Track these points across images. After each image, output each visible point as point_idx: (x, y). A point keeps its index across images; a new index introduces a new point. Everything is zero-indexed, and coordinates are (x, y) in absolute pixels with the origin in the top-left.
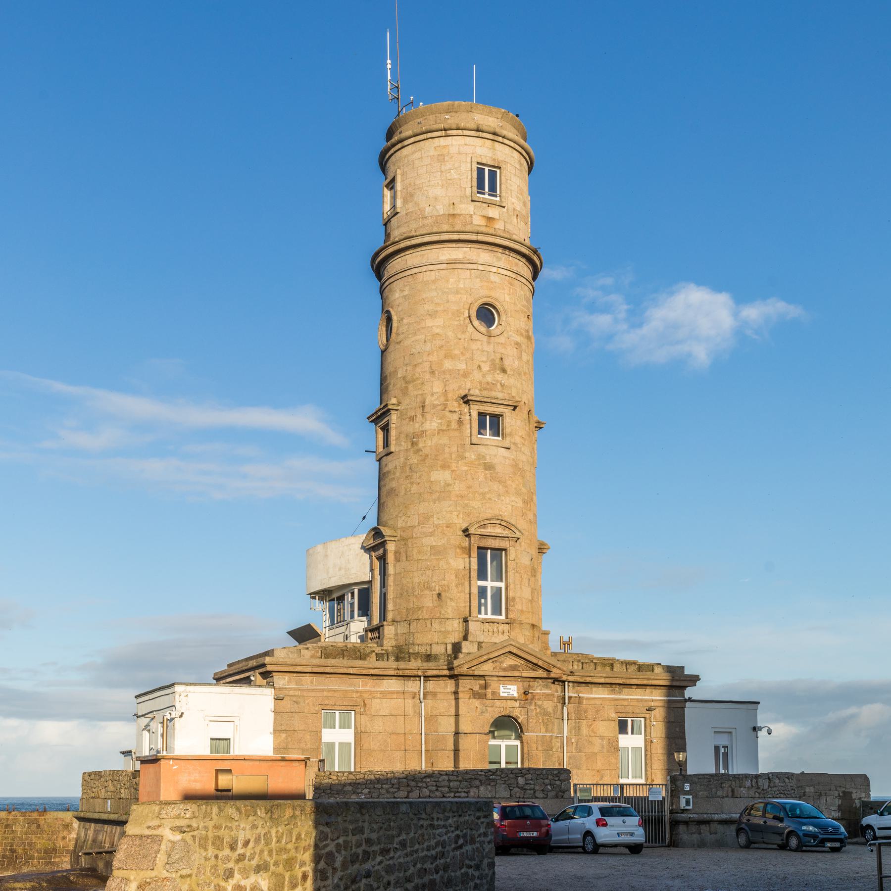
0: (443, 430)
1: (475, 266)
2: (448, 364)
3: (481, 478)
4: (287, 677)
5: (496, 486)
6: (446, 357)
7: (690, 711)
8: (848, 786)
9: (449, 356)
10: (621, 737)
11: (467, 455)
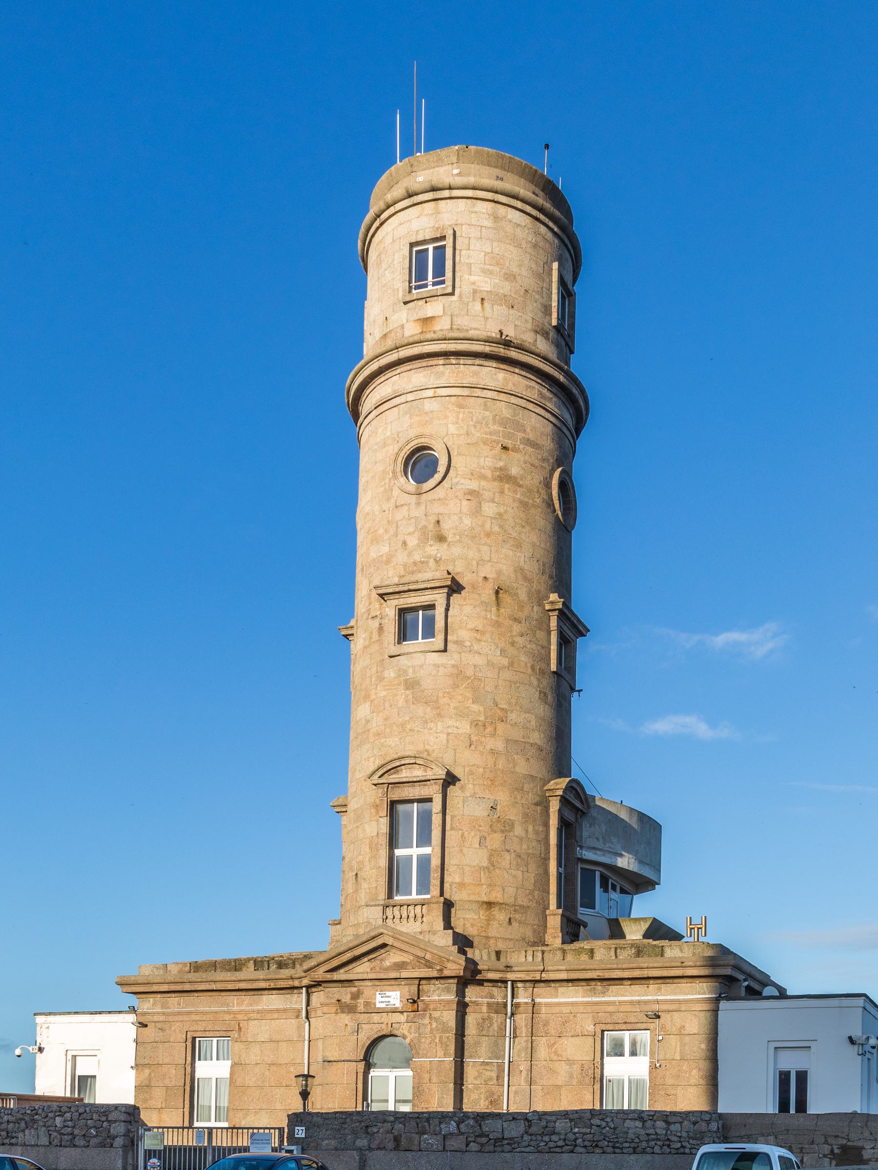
3: (401, 702)
4: (151, 999)
5: (420, 710)
8: (852, 1136)
11: (386, 674)
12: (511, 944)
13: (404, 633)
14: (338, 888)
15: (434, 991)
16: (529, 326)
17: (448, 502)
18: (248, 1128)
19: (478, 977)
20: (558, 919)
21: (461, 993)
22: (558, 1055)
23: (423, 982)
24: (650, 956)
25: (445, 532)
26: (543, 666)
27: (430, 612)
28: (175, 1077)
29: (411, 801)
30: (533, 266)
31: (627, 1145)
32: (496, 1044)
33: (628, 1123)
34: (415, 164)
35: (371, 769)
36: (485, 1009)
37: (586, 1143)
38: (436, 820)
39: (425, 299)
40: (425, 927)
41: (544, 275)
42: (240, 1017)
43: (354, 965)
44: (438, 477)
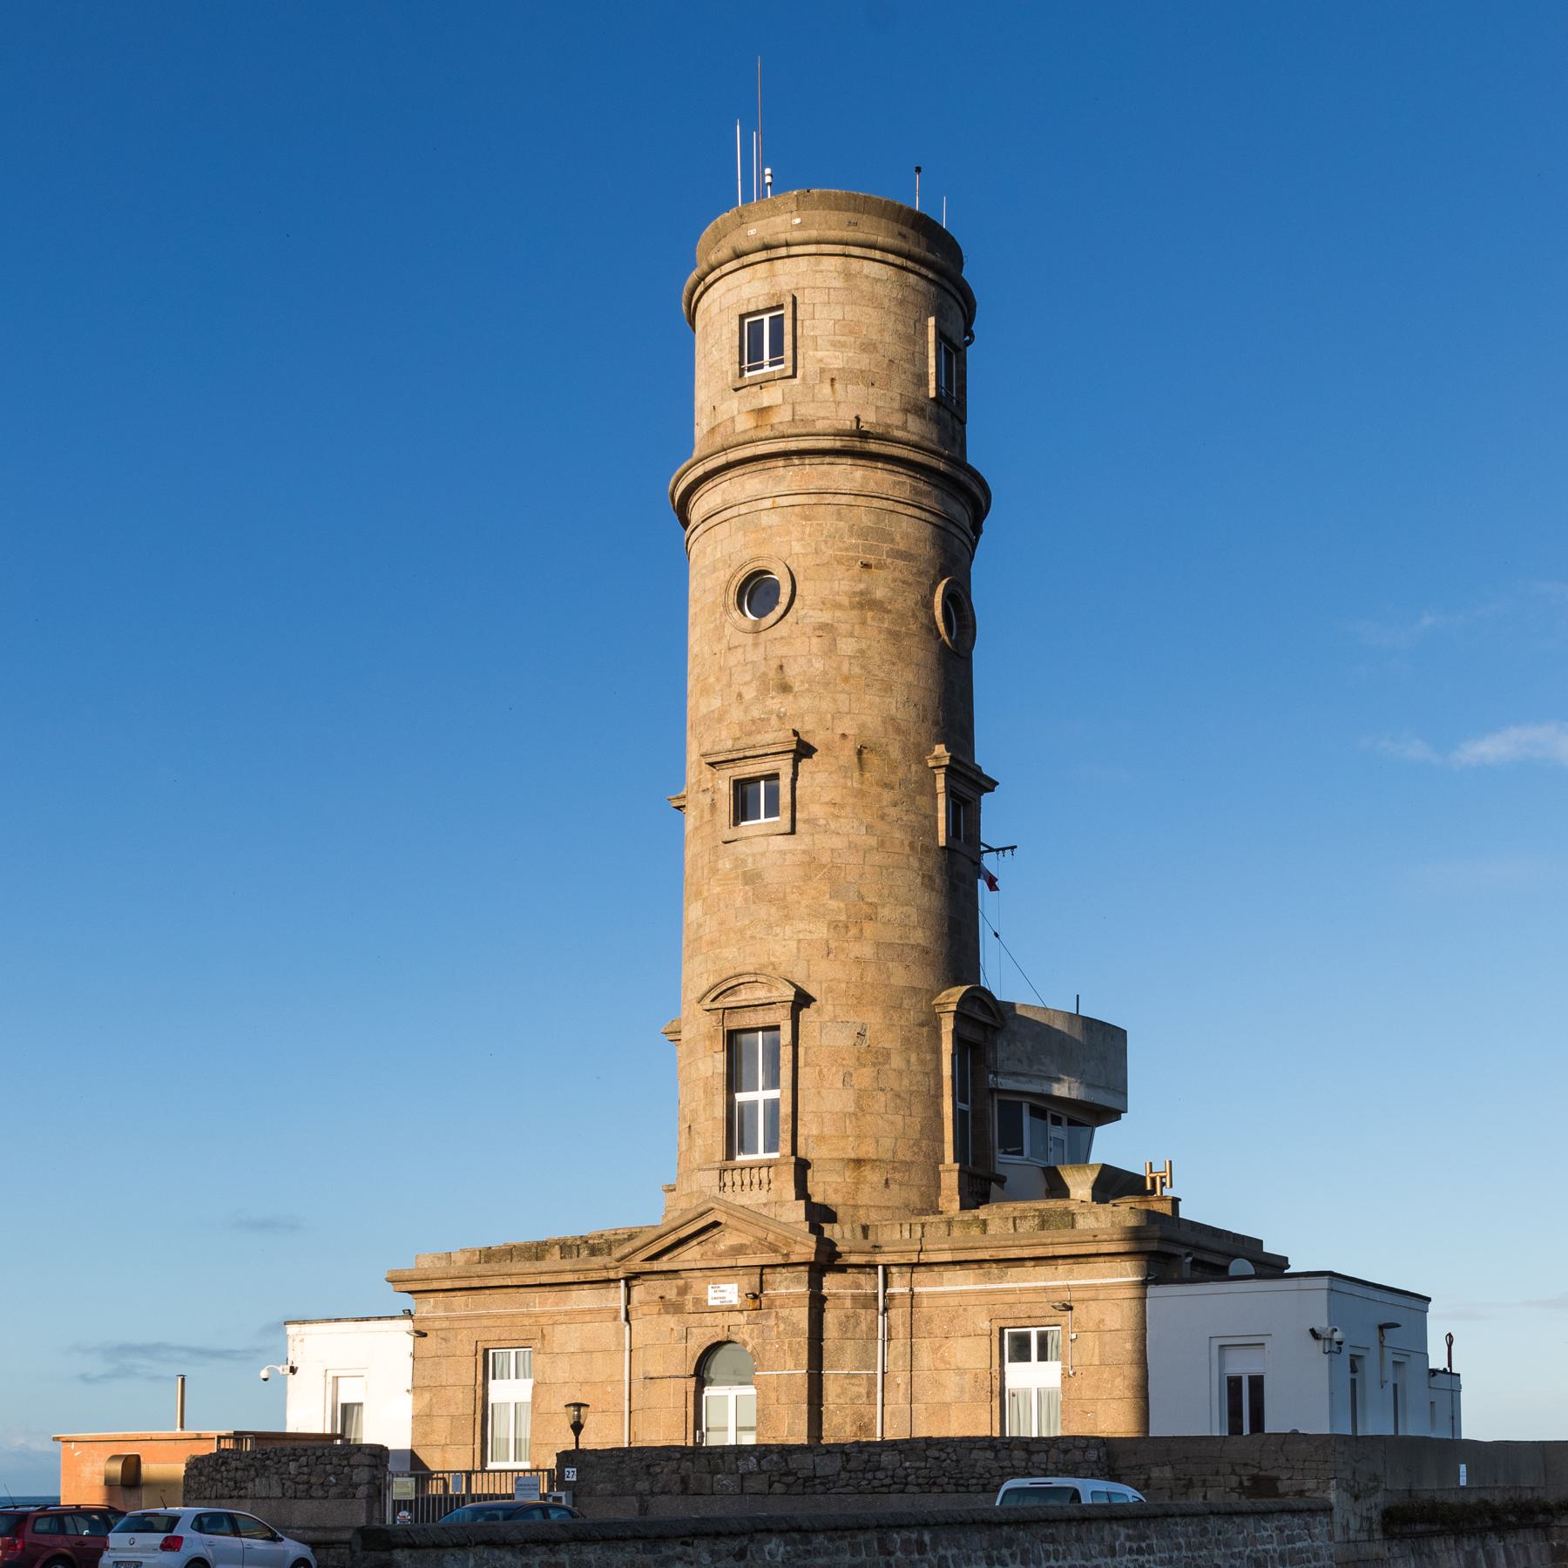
3: (739, 902)
4: (431, 1299)
5: (762, 911)
10: (1012, 1369)
11: (720, 866)
12: (888, 1214)
13: (743, 808)
14: (643, 1153)
16: (896, 405)
17: (794, 639)
19: (839, 1262)
20: (955, 1175)
21: (815, 1284)
23: (766, 1271)
25: (790, 680)
26: (927, 840)
27: (773, 783)
28: (462, 1403)
29: (755, 1030)
30: (900, 327)
31: (974, 1481)
32: (865, 1350)
33: (975, 1454)
35: (705, 988)
36: (848, 1303)
38: (786, 1054)
39: (761, 384)
40: (772, 1196)
41: (914, 338)
42: (543, 1320)
43: (680, 1250)
44: (780, 610)
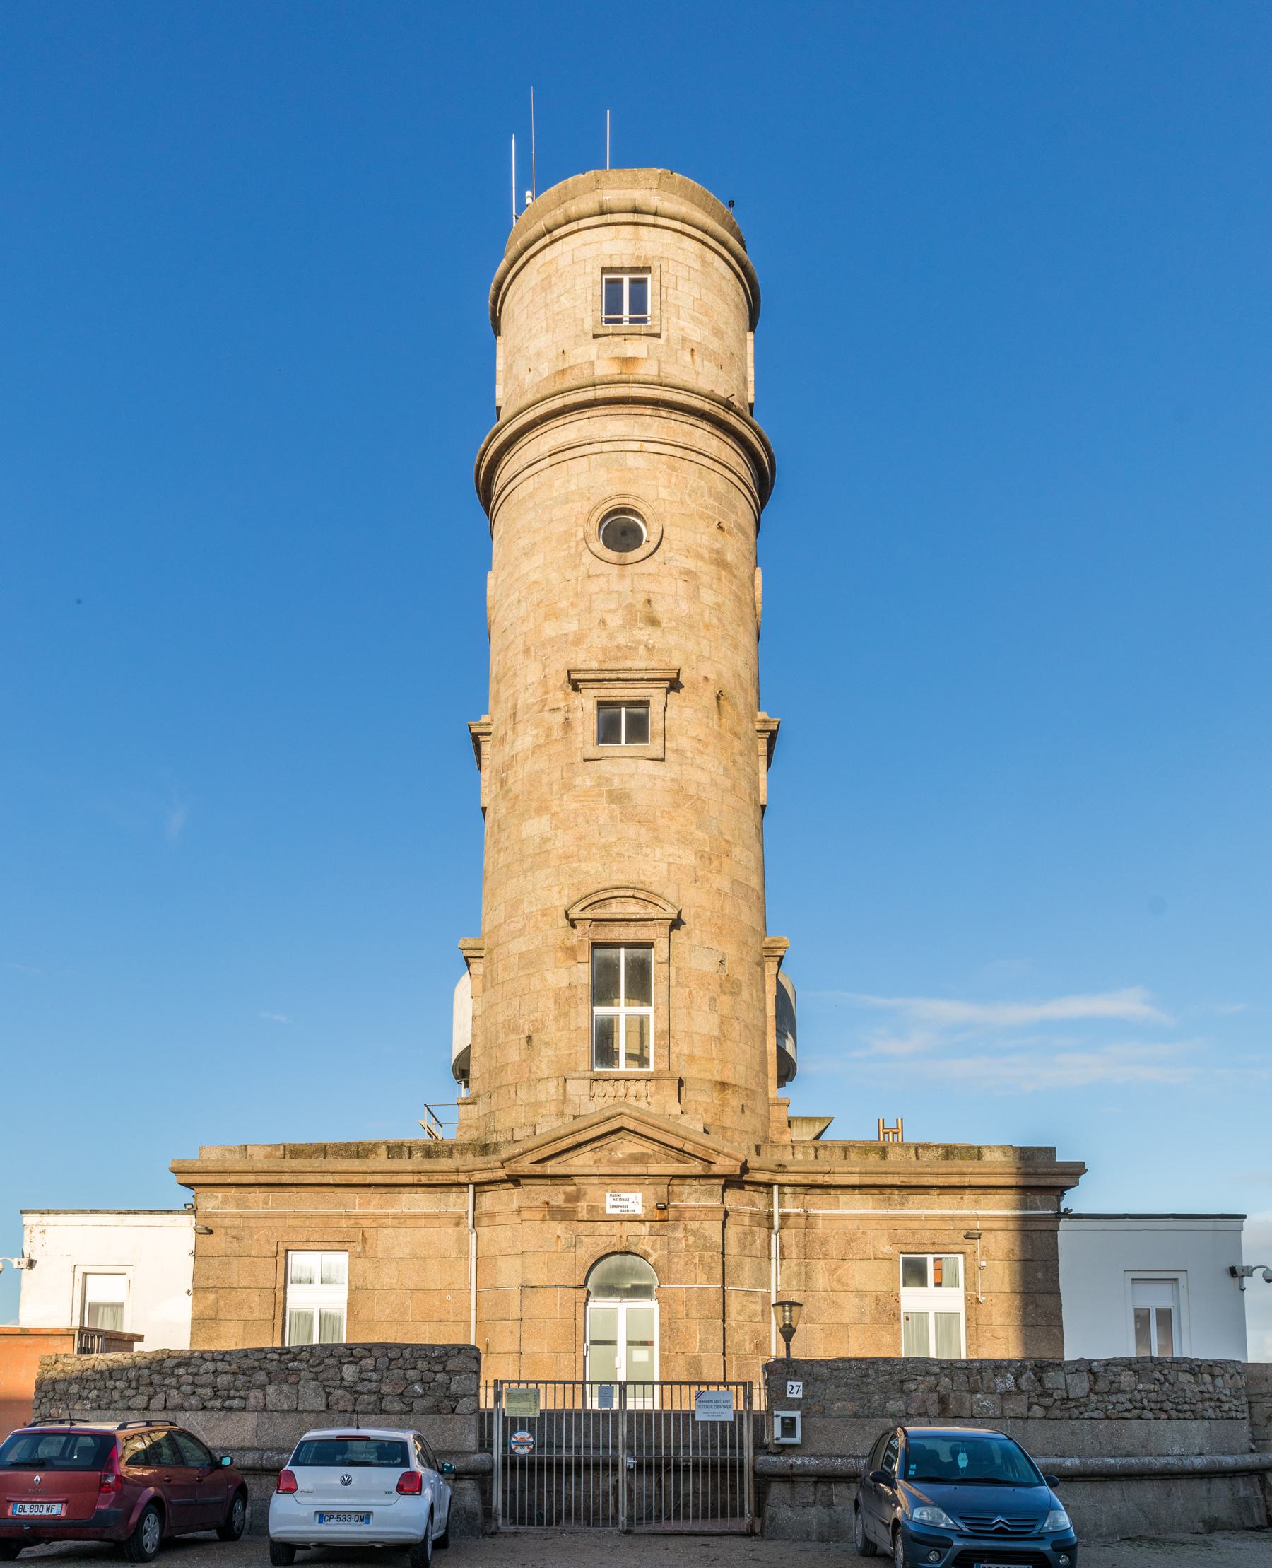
0: (540, 746)
1: (596, 448)
2: (550, 630)
4: (220, 1194)
5: (632, 831)
6: (546, 618)
7: (1066, 1232)
9: (553, 614)
11: (578, 781)
13: (608, 732)
15: (689, 1194)
17: (661, 576)
18: (690, 1384)
22: (843, 1284)
24: (962, 1158)
29: (616, 946)
31: (1187, 1407)
34: (603, 179)
36: (747, 1220)
37: (1152, 1405)
42: (365, 1223)
